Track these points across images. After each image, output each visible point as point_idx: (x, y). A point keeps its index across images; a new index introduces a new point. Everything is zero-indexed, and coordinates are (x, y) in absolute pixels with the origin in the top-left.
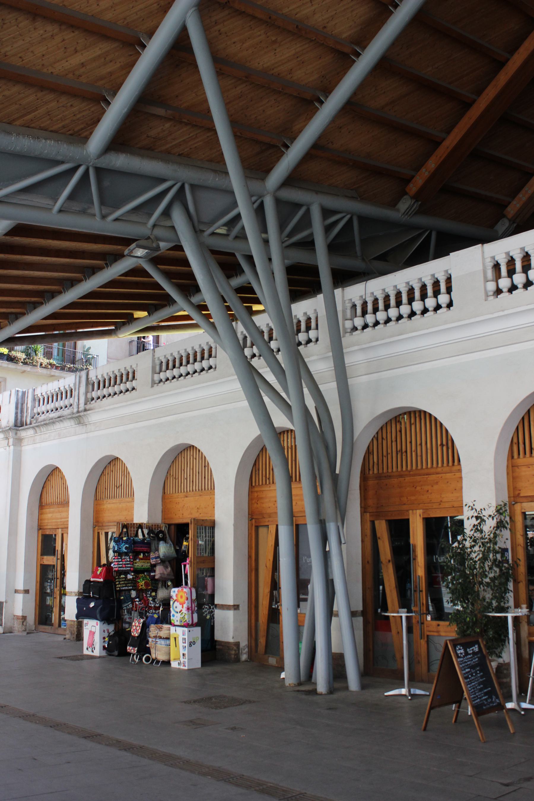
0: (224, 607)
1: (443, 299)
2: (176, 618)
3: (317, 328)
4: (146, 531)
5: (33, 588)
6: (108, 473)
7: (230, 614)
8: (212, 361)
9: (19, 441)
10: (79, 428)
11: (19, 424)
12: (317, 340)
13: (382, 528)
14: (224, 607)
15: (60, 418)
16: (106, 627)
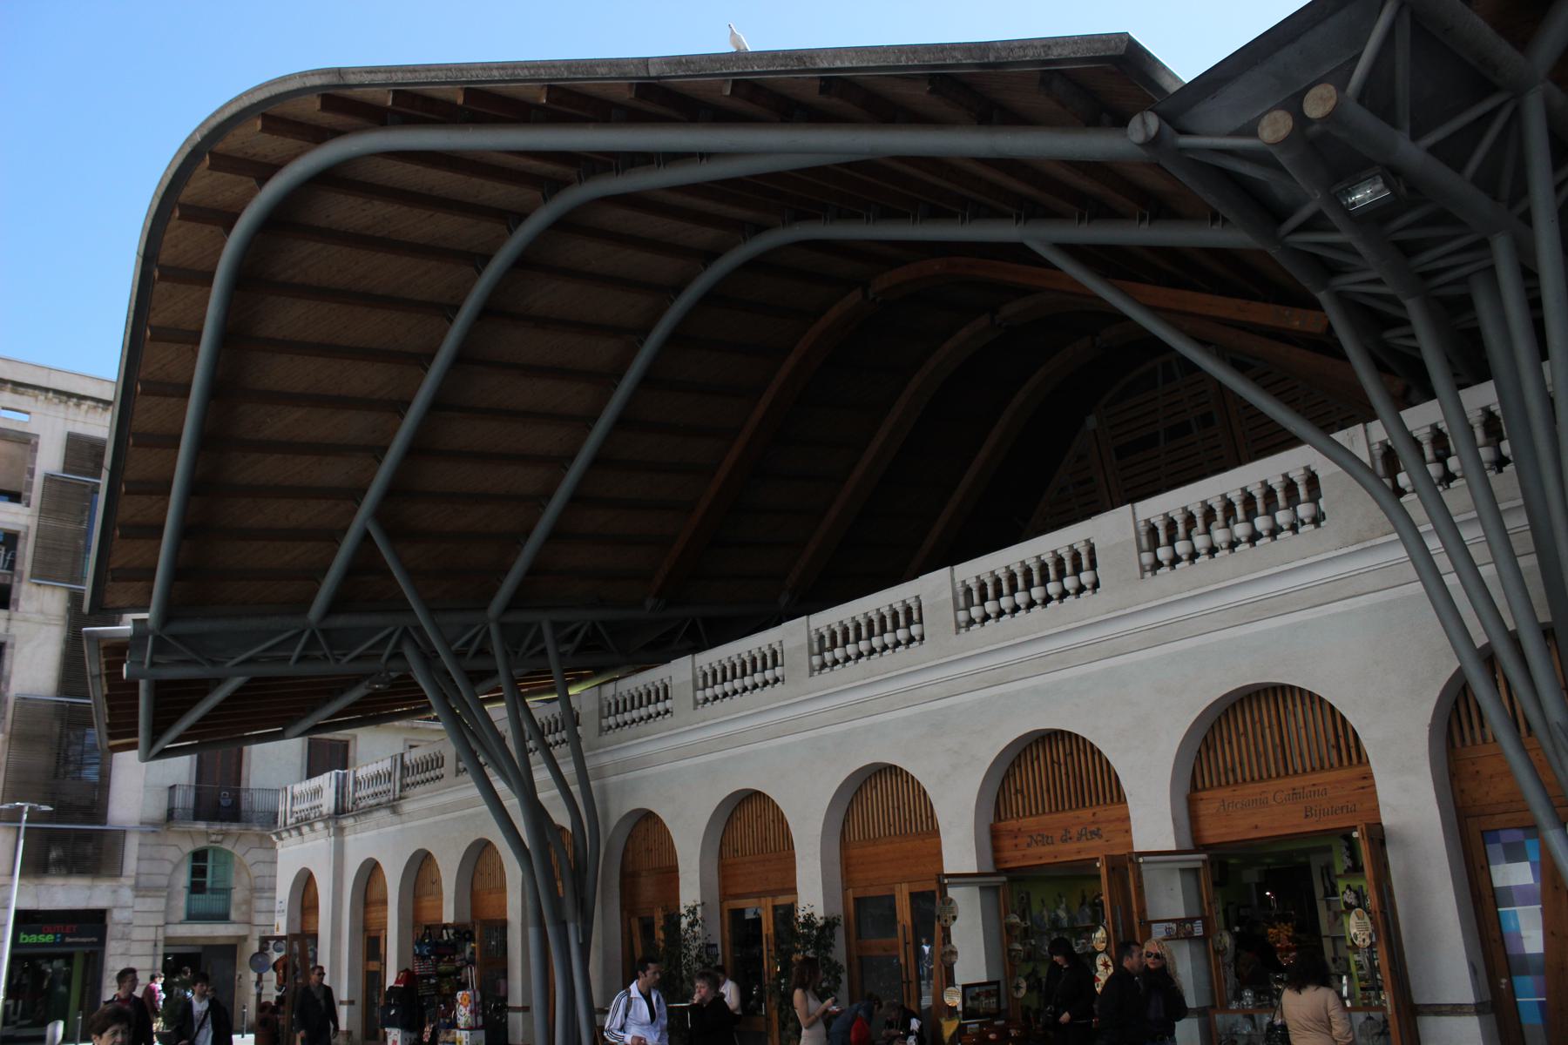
0: (516, 1009)
1: (1086, 577)
2: (462, 1021)
3: (921, 621)
4: (451, 932)
5: (359, 999)
6: (421, 865)
7: (520, 1015)
8: (668, 703)
9: (340, 831)
10: (395, 818)
11: (340, 811)
12: (922, 638)
13: (635, 923)
14: (516, 1009)
15: (379, 806)
16: (408, 1035)
